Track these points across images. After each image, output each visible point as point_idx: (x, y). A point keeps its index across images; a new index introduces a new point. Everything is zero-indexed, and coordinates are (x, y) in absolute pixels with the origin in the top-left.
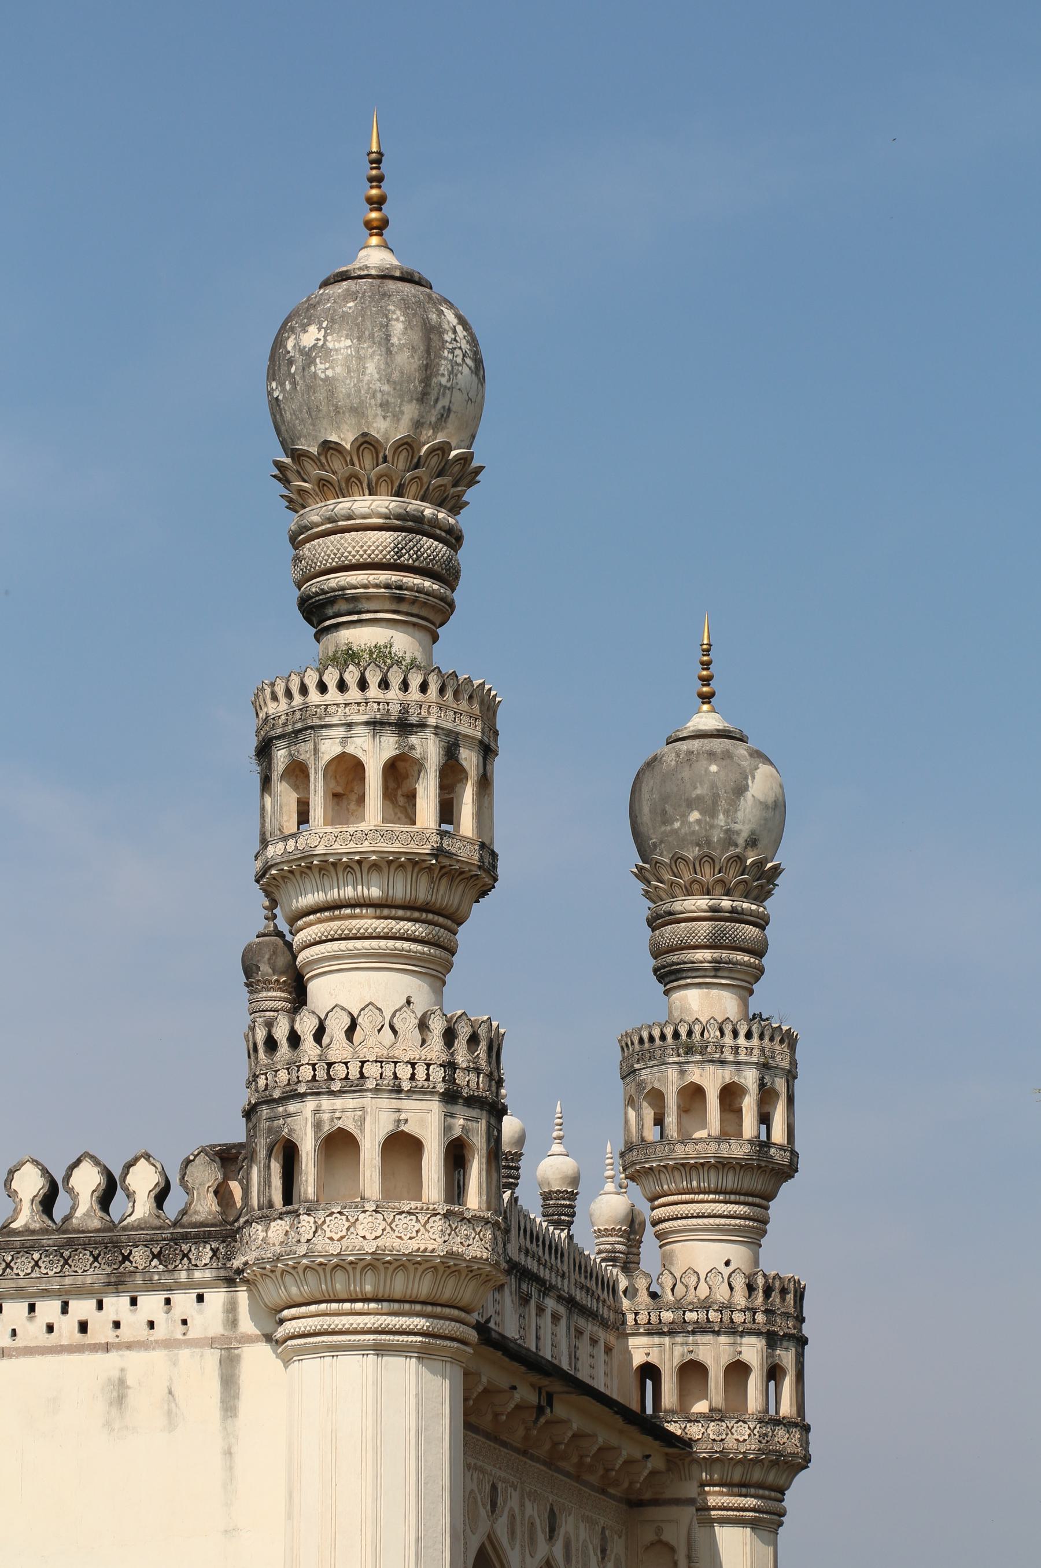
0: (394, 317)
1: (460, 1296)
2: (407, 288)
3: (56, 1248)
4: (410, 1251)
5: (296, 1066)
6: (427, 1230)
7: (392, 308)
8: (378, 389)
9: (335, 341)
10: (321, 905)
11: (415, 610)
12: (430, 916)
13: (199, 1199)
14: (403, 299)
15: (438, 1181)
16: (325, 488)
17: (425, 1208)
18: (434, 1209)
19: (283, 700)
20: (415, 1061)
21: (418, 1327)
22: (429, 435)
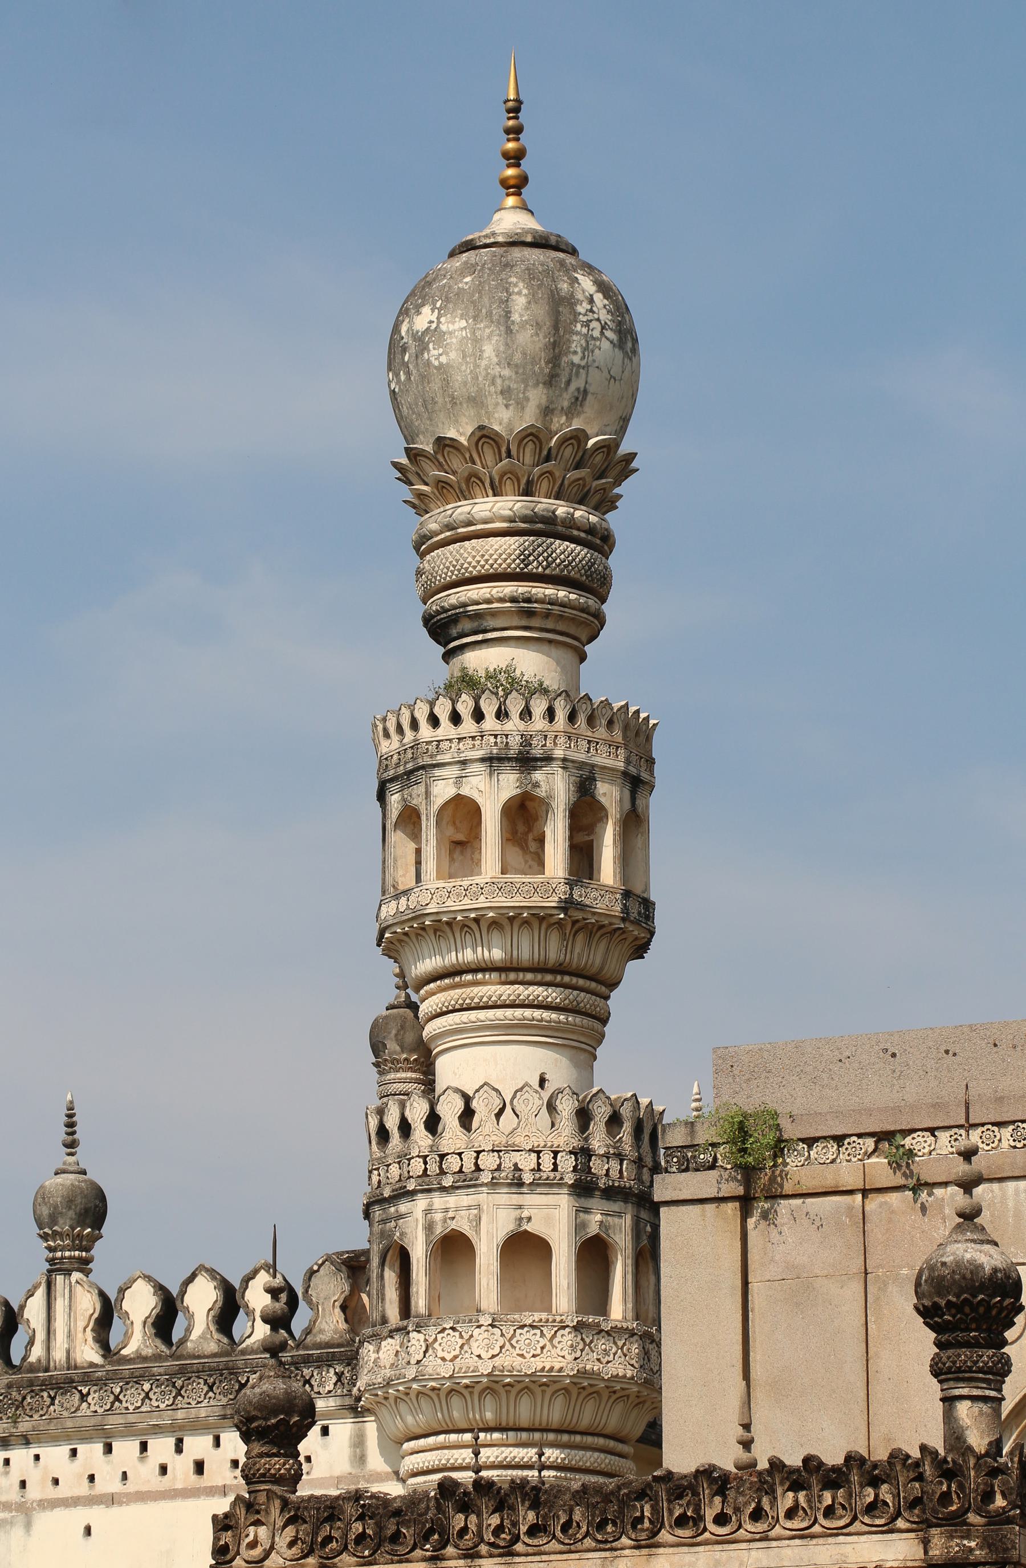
0: (516, 290)
1: (603, 1421)
2: (536, 256)
3: (167, 1377)
4: (534, 1371)
5: (407, 1159)
6: (554, 1346)
7: (513, 280)
8: (497, 374)
9: (448, 323)
10: (440, 971)
11: (550, 625)
12: (567, 979)
13: (324, 1316)
14: (528, 269)
15: (568, 1288)
16: (445, 491)
17: (550, 1320)
18: (561, 1321)
19: (395, 737)
20: (539, 1149)
21: (551, 1460)
22: (562, 422)
